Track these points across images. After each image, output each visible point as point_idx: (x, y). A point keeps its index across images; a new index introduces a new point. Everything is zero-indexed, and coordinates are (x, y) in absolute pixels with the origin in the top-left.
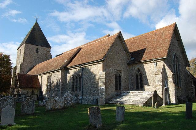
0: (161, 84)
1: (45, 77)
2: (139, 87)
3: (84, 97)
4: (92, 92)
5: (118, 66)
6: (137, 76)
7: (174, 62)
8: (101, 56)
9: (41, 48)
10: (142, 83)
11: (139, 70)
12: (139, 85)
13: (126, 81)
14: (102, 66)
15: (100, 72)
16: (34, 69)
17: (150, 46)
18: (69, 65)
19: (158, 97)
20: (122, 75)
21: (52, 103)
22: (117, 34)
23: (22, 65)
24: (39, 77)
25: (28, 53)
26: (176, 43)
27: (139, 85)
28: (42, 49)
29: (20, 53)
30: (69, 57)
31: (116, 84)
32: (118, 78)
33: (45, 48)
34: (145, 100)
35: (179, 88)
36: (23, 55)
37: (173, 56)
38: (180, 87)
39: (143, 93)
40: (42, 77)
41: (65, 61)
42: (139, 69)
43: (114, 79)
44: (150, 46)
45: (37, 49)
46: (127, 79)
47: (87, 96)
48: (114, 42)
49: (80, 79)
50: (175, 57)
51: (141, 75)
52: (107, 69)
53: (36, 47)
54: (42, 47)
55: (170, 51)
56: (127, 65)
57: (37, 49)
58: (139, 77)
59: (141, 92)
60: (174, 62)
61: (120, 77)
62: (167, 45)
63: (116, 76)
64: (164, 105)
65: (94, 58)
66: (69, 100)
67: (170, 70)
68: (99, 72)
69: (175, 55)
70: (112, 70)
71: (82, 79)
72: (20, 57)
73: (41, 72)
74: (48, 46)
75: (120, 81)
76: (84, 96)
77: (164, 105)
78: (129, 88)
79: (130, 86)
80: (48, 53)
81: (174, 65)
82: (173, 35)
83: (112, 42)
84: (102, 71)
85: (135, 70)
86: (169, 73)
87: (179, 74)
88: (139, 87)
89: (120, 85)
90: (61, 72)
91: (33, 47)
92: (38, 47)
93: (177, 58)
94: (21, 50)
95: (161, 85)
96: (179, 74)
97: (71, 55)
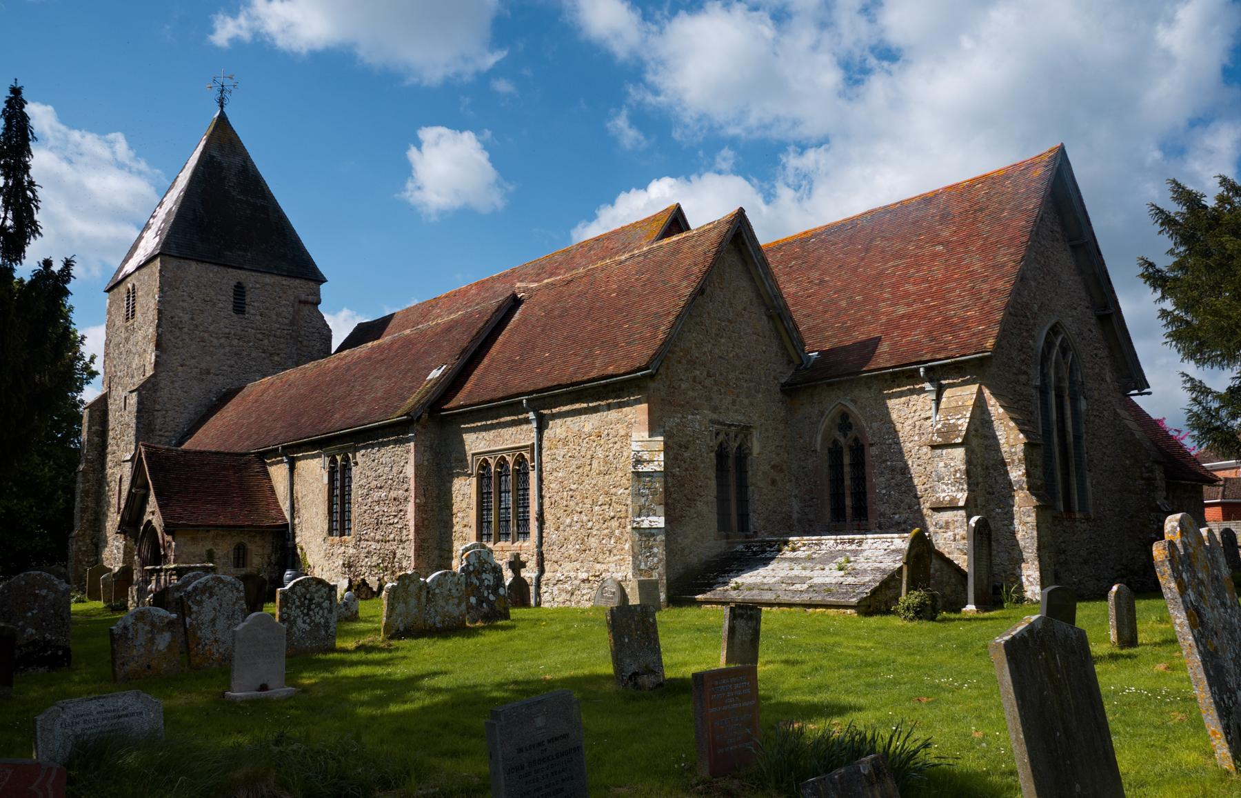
0: (962, 497)
1: (314, 470)
2: (849, 511)
3: (547, 575)
4: (593, 542)
5: (734, 403)
6: (835, 452)
7: (1044, 376)
8: (641, 354)
9: (261, 285)
10: (865, 494)
11: (845, 422)
12: (848, 502)
13: (774, 482)
14: (645, 417)
15: (635, 436)
16: (230, 412)
17: (907, 287)
18: (460, 399)
19: (935, 564)
20: (756, 448)
21: (413, 602)
22: (725, 228)
23: (147, 391)
24: (278, 473)
25: (186, 317)
26: (1063, 262)
27: (848, 502)
28: (265, 288)
29: (130, 314)
30: (457, 350)
31: (722, 500)
32: (731, 463)
33: (285, 282)
34: (870, 580)
35: (1074, 520)
36: (151, 331)
37: (1041, 343)
38: (1083, 508)
39: (865, 546)
40: (292, 469)
41: (435, 374)
42: (845, 416)
43: (712, 474)
44: (907, 287)
45: (239, 290)
46: (781, 471)
47: (568, 566)
48: (708, 275)
49: (522, 475)
50: (1049, 344)
51: (858, 450)
52: (672, 422)
53: (233, 276)
54: (268, 279)
55: (1017, 315)
56: (780, 396)
57: (239, 290)
58: (847, 460)
59: (851, 542)
60: (1044, 376)
61: (742, 457)
62: (1000, 285)
63: (721, 455)
64: (971, 607)
65: (602, 365)
66: (488, 587)
67: (1012, 424)
68: (627, 436)
69: (1054, 331)
70: (698, 422)
71: (533, 476)
72: (127, 340)
73: (279, 435)
74: (305, 272)
75: (742, 485)
76: (547, 566)
77: (971, 607)
78: (795, 516)
79: (796, 506)
80: (306, 310)
81: (1043, 391)
82: (1040, 220)
83: (696, 269)
84: (646, 435)
85: (825, 423)
86: (1010, 439)
87: (1078, 438)
88: (849, 511)
89: (743, 501)
90: (412, 444)
91: (210, 282)
92: (241, 275)
93: (1064, 350)
94: (132, 294)
95: (961, 504)
96: (1078, 438)
97: (463, 339)
